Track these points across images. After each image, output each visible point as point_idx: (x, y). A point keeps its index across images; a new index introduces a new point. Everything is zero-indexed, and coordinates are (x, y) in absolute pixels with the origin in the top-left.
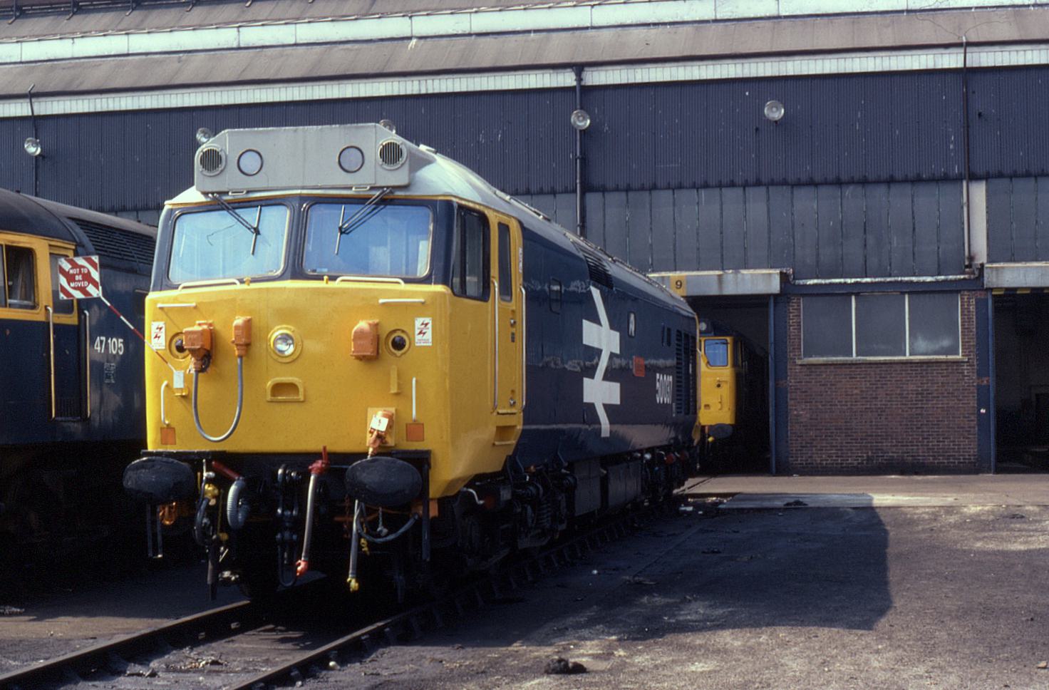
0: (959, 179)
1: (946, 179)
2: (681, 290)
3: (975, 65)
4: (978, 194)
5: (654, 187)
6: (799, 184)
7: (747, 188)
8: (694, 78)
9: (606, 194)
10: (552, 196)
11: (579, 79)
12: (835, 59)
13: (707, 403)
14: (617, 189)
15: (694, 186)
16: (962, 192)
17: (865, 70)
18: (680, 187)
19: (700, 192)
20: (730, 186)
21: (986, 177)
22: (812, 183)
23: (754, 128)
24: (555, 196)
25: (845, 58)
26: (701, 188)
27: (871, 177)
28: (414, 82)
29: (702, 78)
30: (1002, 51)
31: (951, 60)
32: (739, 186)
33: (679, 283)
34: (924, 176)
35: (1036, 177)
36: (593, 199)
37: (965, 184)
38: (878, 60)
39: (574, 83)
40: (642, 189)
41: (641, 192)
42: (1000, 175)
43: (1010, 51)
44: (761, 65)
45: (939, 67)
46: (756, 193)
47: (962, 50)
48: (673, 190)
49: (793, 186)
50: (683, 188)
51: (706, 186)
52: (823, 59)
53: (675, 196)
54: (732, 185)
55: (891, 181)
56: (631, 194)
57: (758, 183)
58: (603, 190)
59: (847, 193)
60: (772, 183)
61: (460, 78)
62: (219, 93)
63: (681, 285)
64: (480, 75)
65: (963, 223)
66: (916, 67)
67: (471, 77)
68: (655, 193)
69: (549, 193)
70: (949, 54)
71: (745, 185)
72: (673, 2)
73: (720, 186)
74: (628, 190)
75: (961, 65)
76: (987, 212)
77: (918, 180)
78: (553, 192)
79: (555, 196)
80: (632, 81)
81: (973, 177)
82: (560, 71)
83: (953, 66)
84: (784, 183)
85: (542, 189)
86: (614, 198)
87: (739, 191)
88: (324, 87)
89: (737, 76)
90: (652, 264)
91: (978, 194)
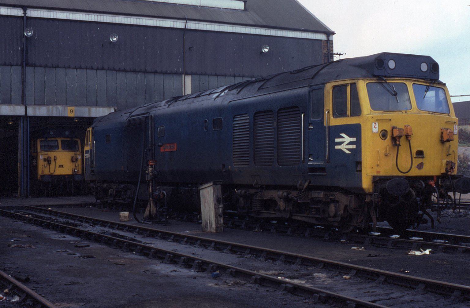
0: (181, 74)
1: (177, 74)
2: (72, 114)
3: (189, 28)
4: (188, 80)
5: (58, 67)
6: (119, 70)
7: (98, 70)
8: (77, 19)
9: (46, 68)
10: (10, 67)
11: (25, 13)
12: (55, 12)
13: (61, 164)
14: (41, 66)
15: (75, 68)
16: (182, 80)
17: (147, 25)
18: (69, 67)
19: (77, 71)
20: (91, 69)
21: (191, 74)
22: (125, 71)
23: (101, 44)
24: (11, 67)
25: (220, 25)
26: (79, 69)
27: (159, 70)
28: (99, 16)
29: (80, 20)
30: (198, 24)
31: (179, 24)
32: (95, 69)
33: (72, 111)
34: (168, 71)
35: (209, 75)
36: (29, 70)
37: (183, 76)
38: (152, 21)
39: (23, 15)
40: (52, 67)
41: (4, 66)
42: (196, 74)
43: (201, 24)
44: (105, 17)
45: (175, 27)
46: (101, 73)
47: (185, 21)
48: (96, 70)
49: (117, 71)
50: (71, 68)
51: (80, 68)
52: (50, 12)
53: (67, 71)
54: (92, 68)
55: (155, 73)
56: (47, 69)
57: (102, 69)
58: (34, 66)
59: (138, 76)
60: (109, 69)
61: (7, 9)
62: (270, 31)
63: (72, 112)
64: (86, 13)
65: (182, 92)
66: (166, 26)
67: (252, 28)
68: (57, 69)
69: (8, 65)
70: (179, 22)
71: (97, 69)
72: (239, 1)
73: (86, 69)
74: (46, 67)
75: (183, 27)
76: (191, 88)
77: (166, 73)
78: (11, 65)
79: (11, 67)
80: (49, 17)
81: (187, 74)
82: (74, 12)
83: (180, 27)
84: (113, 69)
85: (5, 63)
86: (40, 70)
87: (95, 71)
88: (310, 34)
89: (95, 21)
90: (56, 101)
91: (188, 80)
